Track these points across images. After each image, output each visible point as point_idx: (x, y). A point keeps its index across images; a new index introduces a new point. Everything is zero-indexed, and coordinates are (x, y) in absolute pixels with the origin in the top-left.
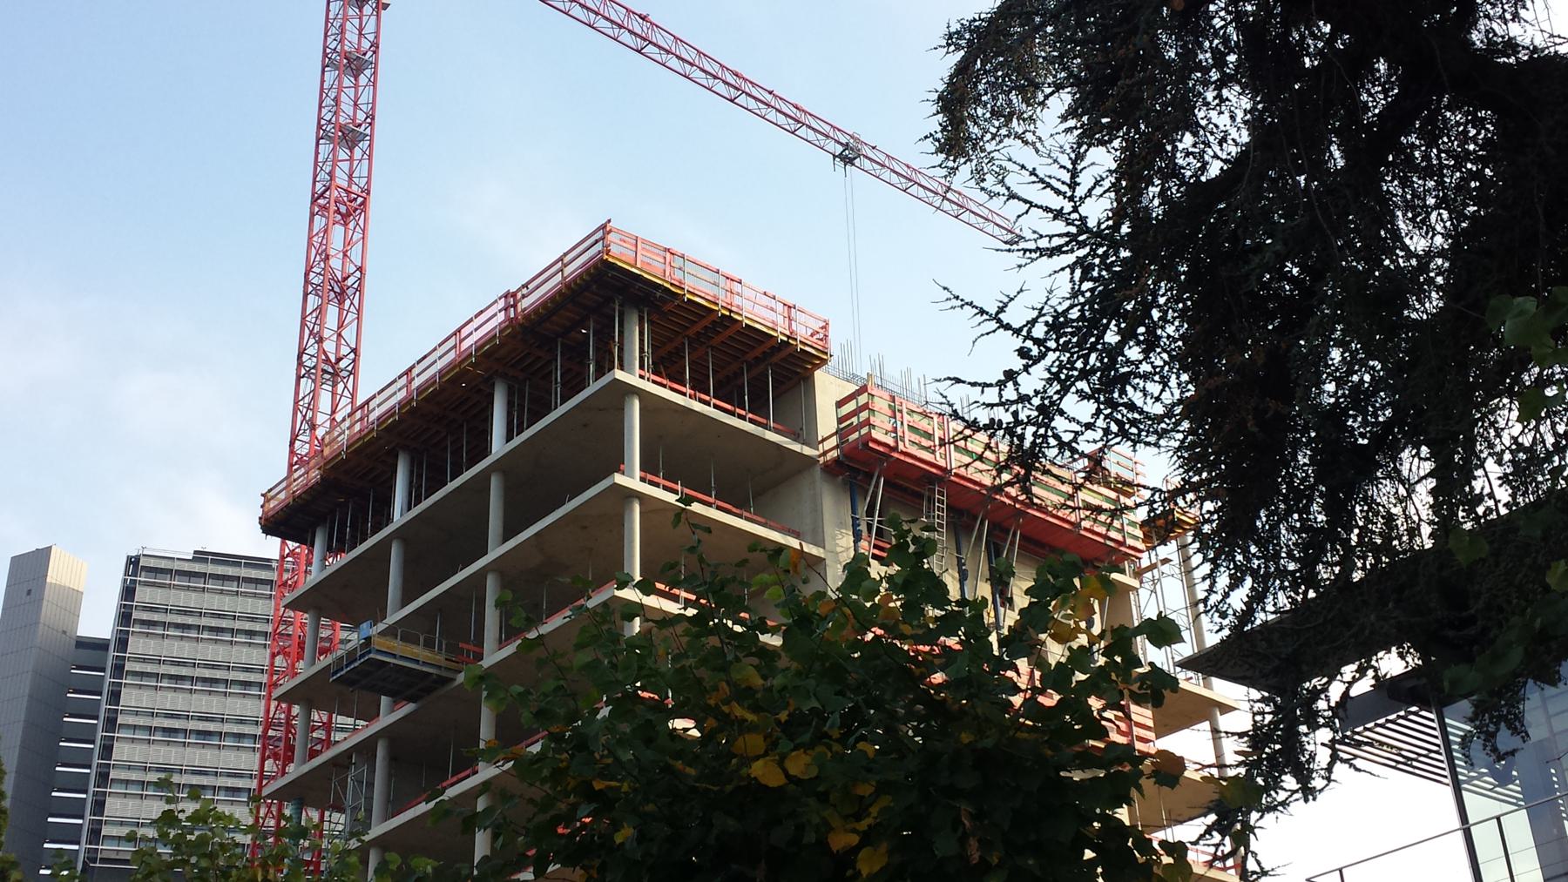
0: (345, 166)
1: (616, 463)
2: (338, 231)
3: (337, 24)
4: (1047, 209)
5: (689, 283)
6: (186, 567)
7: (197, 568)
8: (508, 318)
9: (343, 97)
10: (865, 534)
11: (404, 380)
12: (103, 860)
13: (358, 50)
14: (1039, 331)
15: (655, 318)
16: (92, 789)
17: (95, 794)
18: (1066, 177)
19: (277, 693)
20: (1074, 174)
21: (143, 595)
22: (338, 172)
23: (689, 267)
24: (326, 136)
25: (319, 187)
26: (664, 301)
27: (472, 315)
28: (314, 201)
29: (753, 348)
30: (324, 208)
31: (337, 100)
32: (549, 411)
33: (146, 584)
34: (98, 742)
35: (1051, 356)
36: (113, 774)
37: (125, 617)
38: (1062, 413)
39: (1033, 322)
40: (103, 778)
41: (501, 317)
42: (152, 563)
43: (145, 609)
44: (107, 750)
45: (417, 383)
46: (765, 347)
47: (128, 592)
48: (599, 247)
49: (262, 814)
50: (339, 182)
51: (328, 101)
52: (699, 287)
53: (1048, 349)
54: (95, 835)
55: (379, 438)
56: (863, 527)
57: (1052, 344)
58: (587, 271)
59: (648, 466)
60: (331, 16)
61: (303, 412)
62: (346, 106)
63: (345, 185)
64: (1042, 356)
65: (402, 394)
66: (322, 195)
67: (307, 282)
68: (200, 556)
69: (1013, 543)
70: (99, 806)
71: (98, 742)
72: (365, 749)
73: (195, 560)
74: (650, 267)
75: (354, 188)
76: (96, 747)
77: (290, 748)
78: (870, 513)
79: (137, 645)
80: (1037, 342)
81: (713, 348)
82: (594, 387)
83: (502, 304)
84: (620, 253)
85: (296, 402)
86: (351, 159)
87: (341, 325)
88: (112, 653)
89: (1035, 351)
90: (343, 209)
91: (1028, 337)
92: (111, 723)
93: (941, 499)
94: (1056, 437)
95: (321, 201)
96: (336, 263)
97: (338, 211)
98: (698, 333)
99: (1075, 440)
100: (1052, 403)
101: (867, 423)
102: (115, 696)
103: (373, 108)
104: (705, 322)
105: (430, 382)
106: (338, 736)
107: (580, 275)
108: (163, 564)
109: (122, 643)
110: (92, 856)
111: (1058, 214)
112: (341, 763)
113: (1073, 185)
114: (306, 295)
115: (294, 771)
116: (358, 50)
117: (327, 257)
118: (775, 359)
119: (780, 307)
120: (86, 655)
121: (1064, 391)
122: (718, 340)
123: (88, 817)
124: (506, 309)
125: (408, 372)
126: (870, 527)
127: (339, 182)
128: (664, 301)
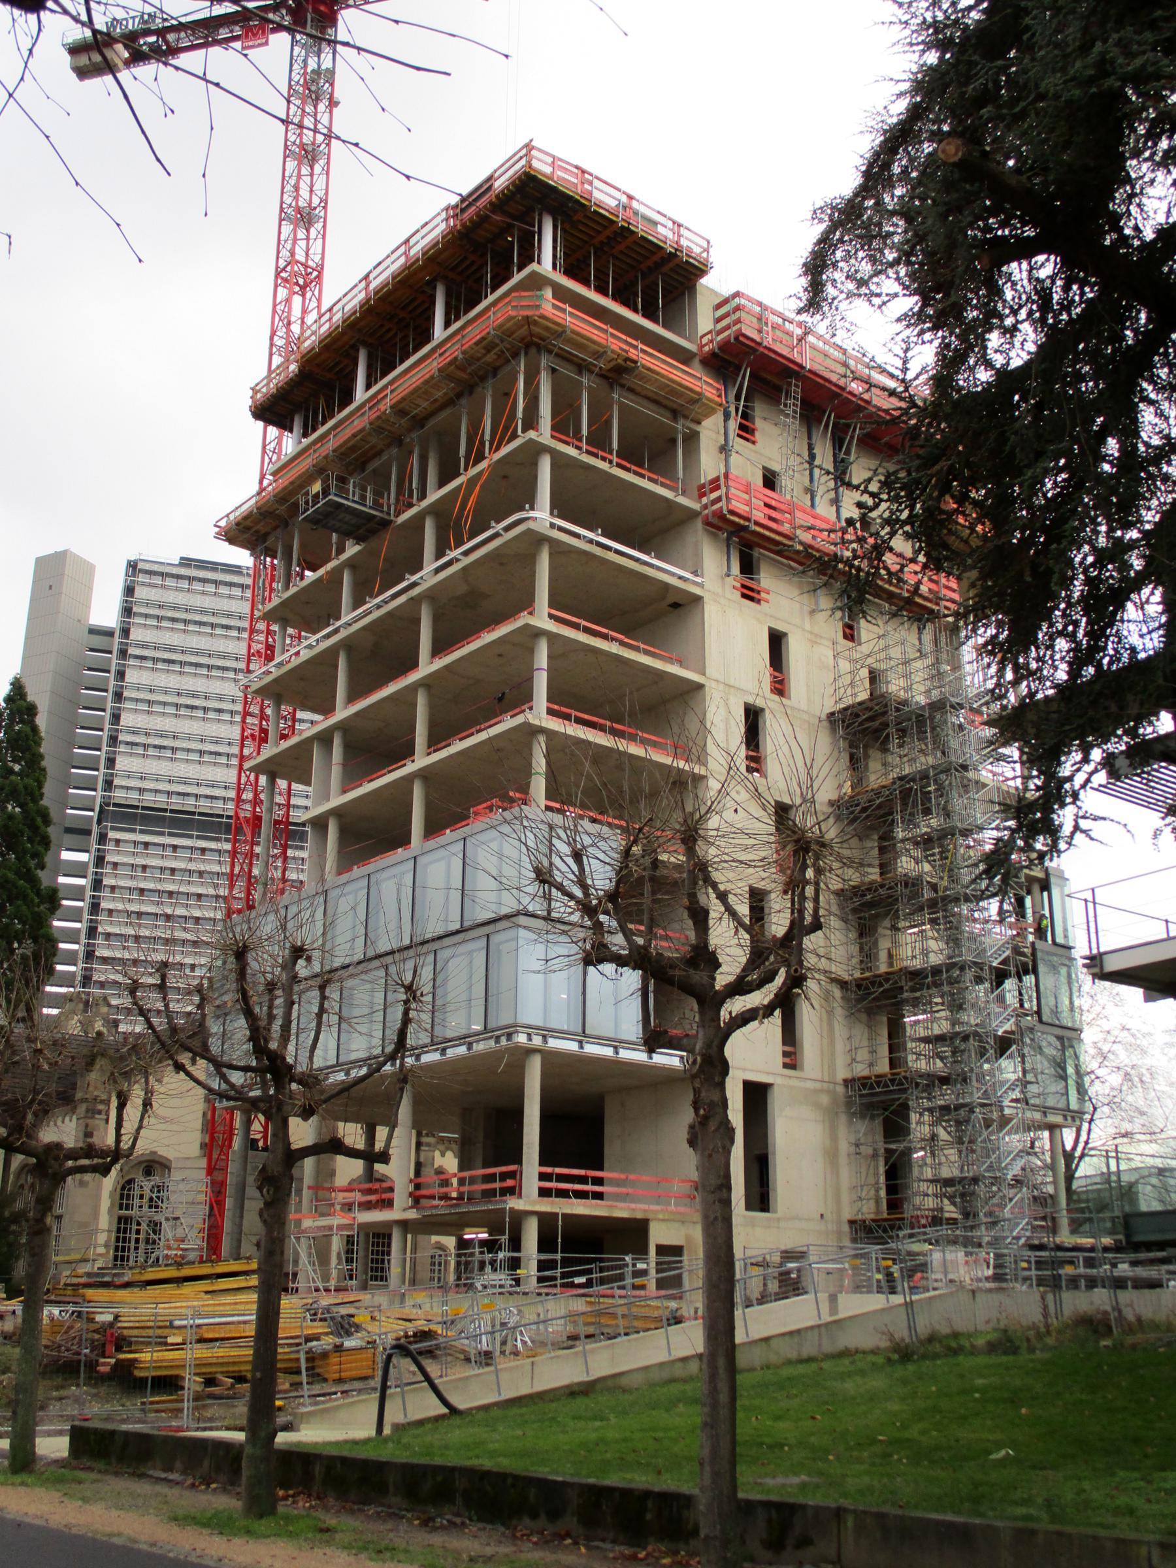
0: (303, 244)
1: (527, 603)
2: (297, 300)
3: (293, 182)
4: (884, 389)
5: (596, 194)
6: (175, 571)
7: (183, 571)
8: (448, 225)
9: (302, 184)
10: (733, 413)
11: (363, 284)
12: (115, 805)
13: (313, 143)
14: (874, 487)
15: (568, 227)
16: (105, 748)
17: (106, 774)
18: (899, 364)
19: (247, 765)
20: (905, 362)
21: (140, 593)
22: (298, 250)
23: (596, 183)
24: (288, 219)
25: (282, 264)
26: (576, 212)
27: (418, 226)
28: (277, 275)
29: (647, 258)
30: (286, 280)
31: (297, 188)
32: (478, 302)
33: (144, 584)
34: (109, 711)
35: (884, 506)
36: (116, 782)
37: (127, 611)
38: (891, 550)
39: (869, 480)
40: (113, 740)
41: (443, 226)
42: (148, 567)
43: (129, 732)
44: (116, 718)
45: (372, 286)
46: (656, 258)
47: (129, 591)
48: (523, 162)
49: (215, 1156)
50: (298, 257)
51: (288, 188)
52: (605, 198)
53: (881, 500)
54: (109, 784)
55: (343, 333)
56: (732, 409)
57: (885, 497)
58: (513, 183)
59: (560, 507)
60: (283, 237)
61: (280, 316)
62: (304, 192)
63: (303, 260)
64: (876, 506)
65: (362, 295)
66: (284, 269)
67: (272, 345)
68: (186, 562)
69: (852, 437)
70: (111, 762)
71: (113, 670)
72: (325, 739)
73: (181, 565)
74: (565, 180)
75: (310, 263)
76: (107, 715)
77: (264, 731)
78: (738, 398)
79: (136, 634)
80: (872, 495)
81: (615, 258)
82: (517, 277)
83: (444, 215)
84: (542, 167)
85: (264, 447)
86: (308, 239)
87: (305, 311)
88: (117, 639)
89: (870, 502)
90: (301, 282)
91: (865, 491)
92: (119, 696)
93: (796, 390)
94: (886, 568)
95: (284, 275)
96: (296, 328)
97: (297, 284)
98: (602, 243)
99: (901, 570)
100: (884, 542)
101: (738, 321)
102: (121, 675)
103: (327, 194)
104: (608, 233)
105: (385, 284)
106: (303, 726)
107: (507, 187)
108: (156, 568)
109: (126, 632)
110: (105, 803)
111: (892, 393)
112: (305, 746)
113: (905, 370)
114: (271, 355)
115: (268, 751)
116: (313, 143)
117: (289, 323)
118: (665, 269)
119: (670, 224)
120: (98, 641)
121: (892, 534)
122: (622, 247)
123: (102, 770)
124: (447, 220)
125: (366, 277)
126: (737, 410)
127: (298, 257)
128: (576, 212)
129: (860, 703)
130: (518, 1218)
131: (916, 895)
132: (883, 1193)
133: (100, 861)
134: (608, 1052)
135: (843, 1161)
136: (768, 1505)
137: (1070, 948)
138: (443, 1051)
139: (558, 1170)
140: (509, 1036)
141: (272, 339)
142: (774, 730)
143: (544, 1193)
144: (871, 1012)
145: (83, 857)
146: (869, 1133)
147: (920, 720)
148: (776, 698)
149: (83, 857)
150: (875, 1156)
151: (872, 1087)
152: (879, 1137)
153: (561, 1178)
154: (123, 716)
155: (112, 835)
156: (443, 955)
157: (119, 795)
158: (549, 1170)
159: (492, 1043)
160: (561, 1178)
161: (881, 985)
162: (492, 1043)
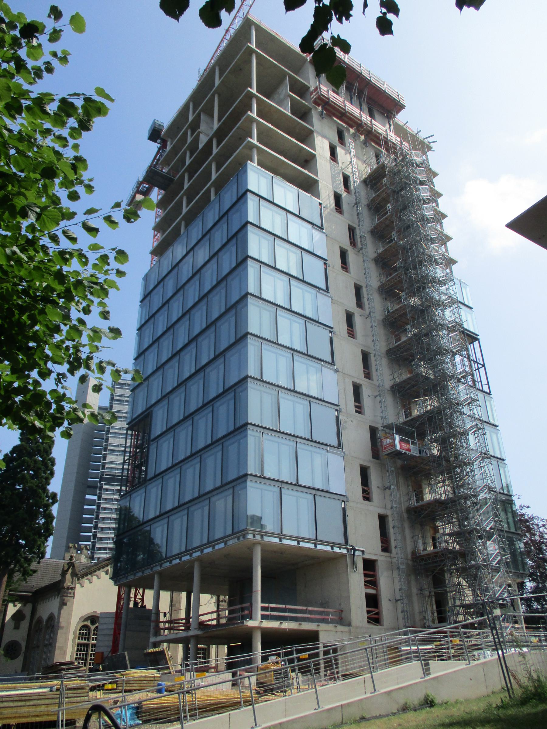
37: (112, 399)
43: (112, 446)
54: (104, 467)
129: (404, 381)
130: (251, 630)
131: (439, 465)
132: (436, 614)
133: (100, 498)
134: (295, 543)
135: (415, 599)
136: (344, 625)
137: (511, 496)
138: (213, 547)
139: (272, 605)
140: (244, 536)
141: (151, 261)
142: (366, 392)
143: (264, 617)
144: (422, 525)
145: (95, 497)
146: (427, 583)
147: (435, 386)
148: (366, 380)
149: (95, 497)
150: (430, 596)
151: (426, 560)
152: (431, 586)
153: (273, 609)
154: (110, 439)
155: (105, 487)
156: (213, 499)
157: (107, 471)
158: (266, 605)
159: (236, 540)
160: (273, 609)
161: (426, 510)
162: (236, 540)
